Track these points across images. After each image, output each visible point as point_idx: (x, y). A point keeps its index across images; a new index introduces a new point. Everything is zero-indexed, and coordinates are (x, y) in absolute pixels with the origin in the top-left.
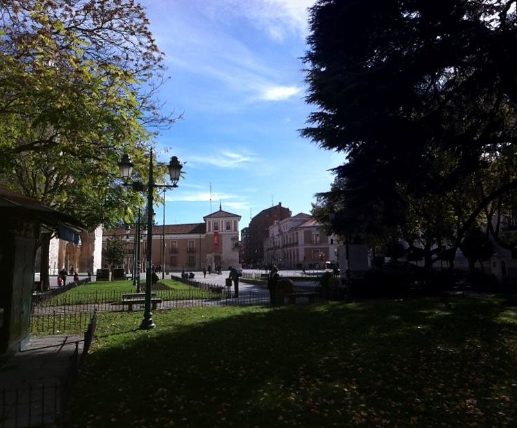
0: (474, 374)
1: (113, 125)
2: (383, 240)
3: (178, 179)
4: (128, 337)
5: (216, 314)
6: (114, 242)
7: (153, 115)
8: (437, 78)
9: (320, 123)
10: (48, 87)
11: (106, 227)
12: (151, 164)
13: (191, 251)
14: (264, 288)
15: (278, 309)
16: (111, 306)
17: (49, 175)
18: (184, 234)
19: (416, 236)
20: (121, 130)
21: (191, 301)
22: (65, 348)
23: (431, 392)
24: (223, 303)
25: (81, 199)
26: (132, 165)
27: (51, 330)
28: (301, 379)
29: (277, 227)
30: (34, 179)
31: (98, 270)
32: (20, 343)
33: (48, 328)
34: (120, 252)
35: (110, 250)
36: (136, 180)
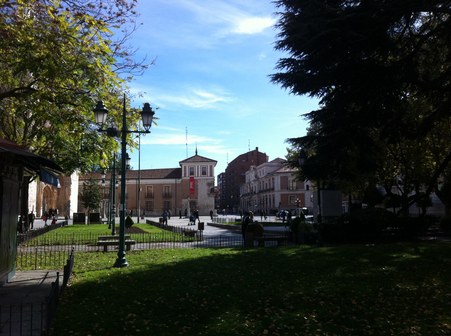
0: (424, 307)
1: (88, 73)
2: (360, 186)
3: (150, 126)
4: (103, 273)
5: (187, 255)
6: (90, 187)
7: (126, 61)
8: (413, 21)
9: (289, 69)
10: (28, 37)
11: (83, 171)
12: (124, 111)
13: (167, 196)
14: (236, 232)
15: (247, 251)
16: (87, 248)
17: (28, 121)
18: (160, 178)
19: (394, 182)
20: (96, 78)
21: (163, 244)
22: (47, 281)
23: (382, 320)
24: (195, 246)
25: (59, 144)
26: (106, 111)
27: (34, 266)
28: (266, 309)
29: (254, 172)
30: (14, 125)
31: (74, 214)
32: (7, 274)
33: (31, 264)
34: (96, 197)
35: (86, 194)
36: (110, 125)
